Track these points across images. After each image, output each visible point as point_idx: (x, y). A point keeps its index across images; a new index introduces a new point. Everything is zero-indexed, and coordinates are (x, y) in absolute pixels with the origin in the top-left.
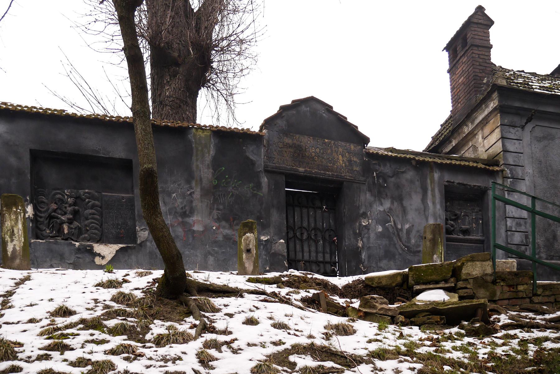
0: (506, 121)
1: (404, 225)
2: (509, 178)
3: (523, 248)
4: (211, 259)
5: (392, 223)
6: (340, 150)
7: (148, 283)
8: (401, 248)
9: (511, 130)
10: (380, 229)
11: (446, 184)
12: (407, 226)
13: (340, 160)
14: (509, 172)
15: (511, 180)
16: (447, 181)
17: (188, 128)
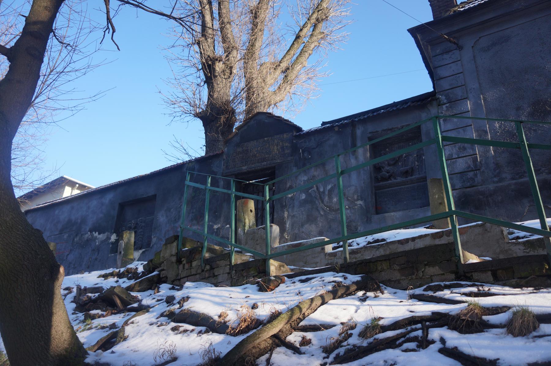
0: (438, 51)
1: (326, 187)
2: (445, 104)
3: (471, 174)
4: (71, 271)
5: (315, 188)
6: (276, 141)
7: (132, 323)
8: (323, 209)
9: (445, 56)
10: (303, 196)
11: (370, 135)
12: (329, 187)
13: (275, 149)
14: (444, 98)
15: (448, 105)
16: (370, 133)
17: (117, 332)
